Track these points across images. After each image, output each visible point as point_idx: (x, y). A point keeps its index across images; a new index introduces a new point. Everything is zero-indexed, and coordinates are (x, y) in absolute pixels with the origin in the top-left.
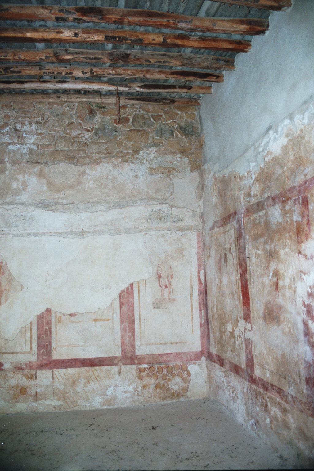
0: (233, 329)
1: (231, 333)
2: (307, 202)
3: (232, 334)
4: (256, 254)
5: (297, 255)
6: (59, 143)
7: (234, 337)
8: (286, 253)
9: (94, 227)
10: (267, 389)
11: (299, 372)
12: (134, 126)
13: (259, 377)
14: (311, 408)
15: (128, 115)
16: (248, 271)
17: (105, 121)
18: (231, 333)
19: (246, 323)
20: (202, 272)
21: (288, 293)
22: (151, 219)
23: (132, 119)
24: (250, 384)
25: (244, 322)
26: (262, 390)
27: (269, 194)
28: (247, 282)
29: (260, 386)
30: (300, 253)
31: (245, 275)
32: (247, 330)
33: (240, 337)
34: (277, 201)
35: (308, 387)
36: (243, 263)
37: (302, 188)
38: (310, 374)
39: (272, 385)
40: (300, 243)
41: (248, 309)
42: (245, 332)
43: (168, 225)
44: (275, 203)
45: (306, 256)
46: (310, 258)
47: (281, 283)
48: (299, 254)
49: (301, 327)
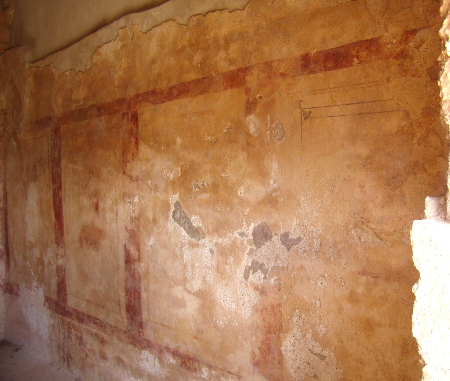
0: (41, 255)
1: (39, 259)
3: (41, 261)
4: (73, 169)
7: (43, 264)
8: (109, 171)
11: (119, 300)
13: (73, 309)
14: (131, 336)
16: (63, 189)
18: (39, 259)
19: (58, 247)
21: (109, 215)
24: (61, 316)
25: (56, 247)
26: (77, 323)
27: (94, 102)
28: (60, 200)
29: (74, 318)
30: (124, 173)
32: (59, 256)
33: (50, 263)
35: (128, 315)
38: (131, 302)
39: (89, 316)
40: (125, 162)
42: (57, 258)
46: (135, 180)
47: (101, 205)
48: (124, 175)
49: (122, 253)
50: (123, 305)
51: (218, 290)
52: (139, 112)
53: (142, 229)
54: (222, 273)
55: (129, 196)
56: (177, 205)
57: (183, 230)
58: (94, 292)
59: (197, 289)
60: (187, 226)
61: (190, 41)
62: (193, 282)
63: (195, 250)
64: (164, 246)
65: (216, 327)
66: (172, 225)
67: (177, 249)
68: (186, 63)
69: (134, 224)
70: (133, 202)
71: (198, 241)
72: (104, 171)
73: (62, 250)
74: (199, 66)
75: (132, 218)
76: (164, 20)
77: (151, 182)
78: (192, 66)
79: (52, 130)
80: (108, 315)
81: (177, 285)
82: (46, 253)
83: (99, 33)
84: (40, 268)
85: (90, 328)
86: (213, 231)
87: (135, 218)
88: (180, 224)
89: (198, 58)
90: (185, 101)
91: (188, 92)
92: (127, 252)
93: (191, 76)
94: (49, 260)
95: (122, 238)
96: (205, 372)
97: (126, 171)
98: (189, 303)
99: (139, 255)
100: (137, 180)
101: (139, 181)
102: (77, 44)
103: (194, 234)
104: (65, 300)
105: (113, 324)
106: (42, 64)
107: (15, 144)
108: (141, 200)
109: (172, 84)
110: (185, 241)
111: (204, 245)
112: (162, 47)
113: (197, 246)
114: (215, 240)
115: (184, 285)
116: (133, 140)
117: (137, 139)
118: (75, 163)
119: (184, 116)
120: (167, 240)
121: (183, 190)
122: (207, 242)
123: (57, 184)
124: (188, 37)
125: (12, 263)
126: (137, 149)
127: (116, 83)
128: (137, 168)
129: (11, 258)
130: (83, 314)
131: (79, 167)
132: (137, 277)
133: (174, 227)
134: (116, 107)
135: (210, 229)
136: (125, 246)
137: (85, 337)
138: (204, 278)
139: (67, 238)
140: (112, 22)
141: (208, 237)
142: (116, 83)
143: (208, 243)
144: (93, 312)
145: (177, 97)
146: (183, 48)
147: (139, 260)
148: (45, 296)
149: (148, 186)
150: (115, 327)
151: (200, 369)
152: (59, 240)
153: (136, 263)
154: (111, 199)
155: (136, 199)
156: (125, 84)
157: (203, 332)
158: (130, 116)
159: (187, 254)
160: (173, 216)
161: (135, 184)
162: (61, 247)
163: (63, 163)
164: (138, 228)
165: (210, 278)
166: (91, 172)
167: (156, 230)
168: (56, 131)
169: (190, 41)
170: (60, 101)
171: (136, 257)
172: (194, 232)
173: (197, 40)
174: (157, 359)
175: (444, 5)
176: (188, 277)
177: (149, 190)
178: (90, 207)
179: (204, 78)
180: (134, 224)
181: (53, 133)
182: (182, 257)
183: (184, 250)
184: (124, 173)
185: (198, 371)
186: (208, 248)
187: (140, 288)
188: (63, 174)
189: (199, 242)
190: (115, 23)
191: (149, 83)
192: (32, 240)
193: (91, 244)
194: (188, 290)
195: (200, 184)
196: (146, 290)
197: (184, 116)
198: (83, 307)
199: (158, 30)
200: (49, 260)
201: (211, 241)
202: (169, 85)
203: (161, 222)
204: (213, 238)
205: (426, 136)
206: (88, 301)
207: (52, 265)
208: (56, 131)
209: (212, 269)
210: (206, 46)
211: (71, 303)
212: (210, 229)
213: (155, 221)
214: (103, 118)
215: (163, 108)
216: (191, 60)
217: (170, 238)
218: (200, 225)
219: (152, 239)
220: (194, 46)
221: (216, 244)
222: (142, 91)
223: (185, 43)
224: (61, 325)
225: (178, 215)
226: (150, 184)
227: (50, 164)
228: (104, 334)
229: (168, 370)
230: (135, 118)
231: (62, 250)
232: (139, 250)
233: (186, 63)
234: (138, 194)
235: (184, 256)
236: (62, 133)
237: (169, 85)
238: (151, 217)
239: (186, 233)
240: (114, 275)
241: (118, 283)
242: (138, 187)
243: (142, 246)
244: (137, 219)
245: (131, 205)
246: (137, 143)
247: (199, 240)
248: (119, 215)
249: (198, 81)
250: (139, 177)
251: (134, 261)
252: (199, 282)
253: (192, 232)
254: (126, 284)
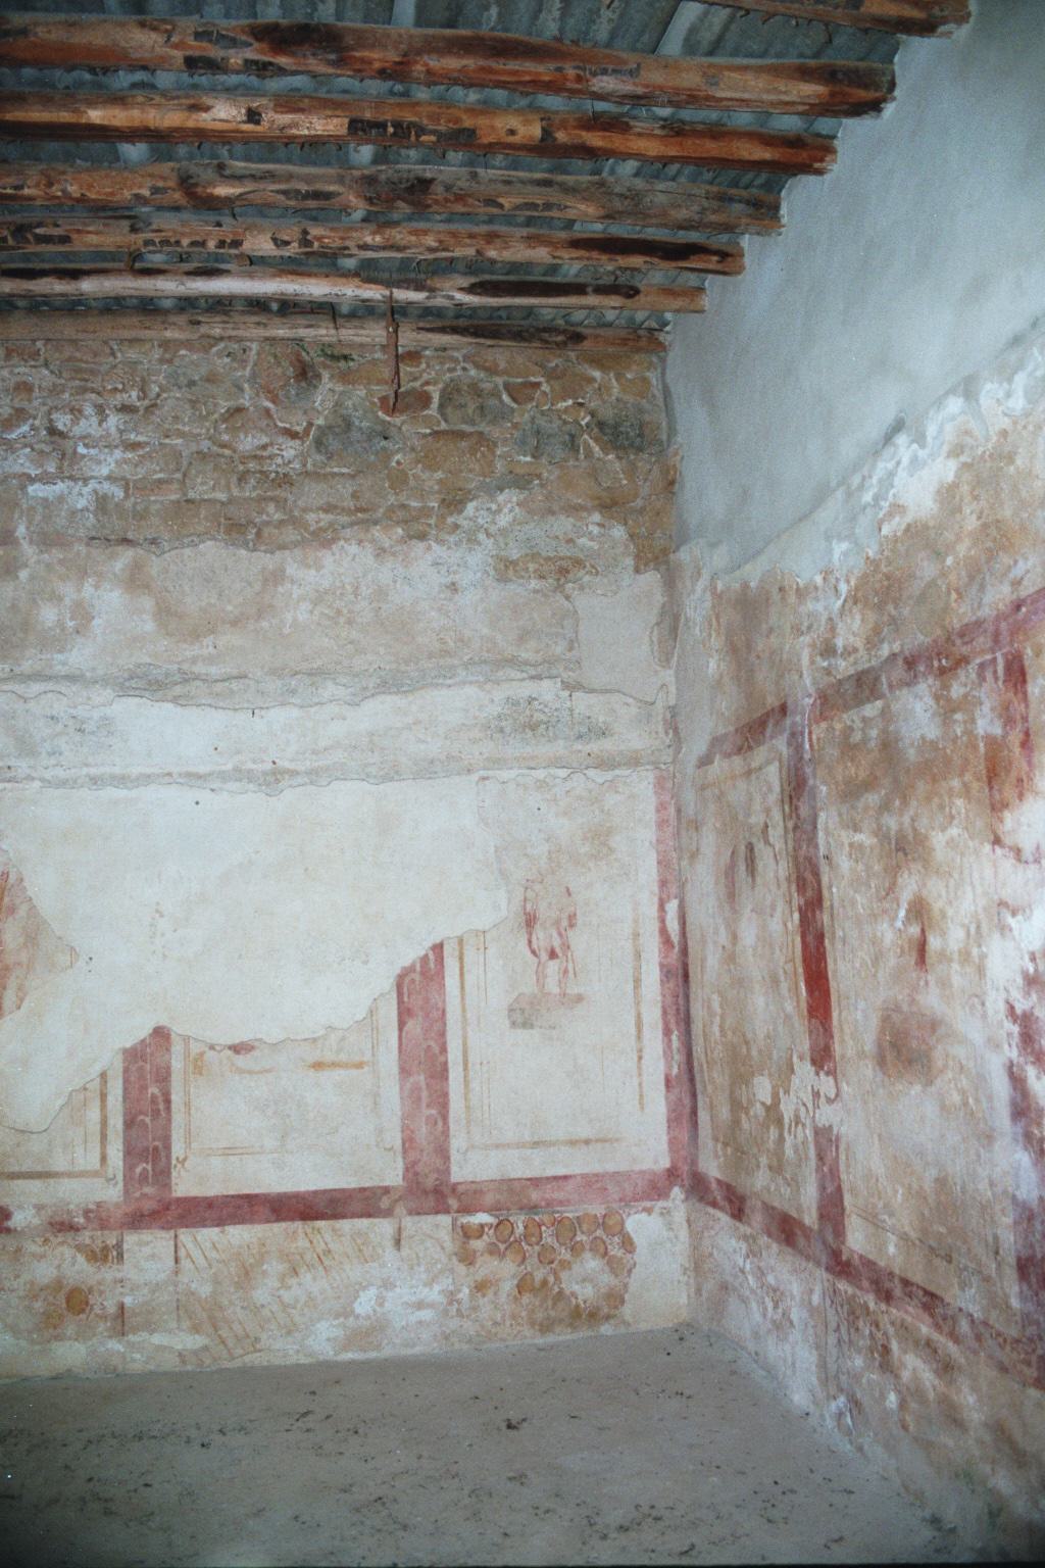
0: (775, 1096)
1: (768, 1109)
2: (1023, 673)
3: (773, 1111)
4: (851, 845)
5: (987, 847)
6: (197, 476)
7: (779, 1121)
8: (951, 843)
9: (314, 757)
10: (887, 1297)
11: (996, 1238)
12: (446, 421)
13: (861, 1257)
14: (1034, 1359)
15: (427, 383)
16: (826, 904)
17: (350, 403)
18: (768, 1109)
19: (817, 1074)
20: (672, 907)
21: (958, 977)
22: (502, 730)
23: (441, 397)
24: (831, 1277)
25: (812, 1073)
26: (870, 1300)
27: (896, 647)
28: (820, 937)
29: (866, 1284)
30: (997, 841)
31: (814, 916)
32: (823, 1099)
33: (797, 1121)
34: (922, 668)
35: (1025, 1288)
36: (809, 876)
37: (1003, 625)
38: (1032, 1246)
39: (906, 1283)
40: (997, 807)
41: (826, 1030)
42: (816, 1106)
43: (559, 748)
44: (915, 676)
45: (1018, 852)
46: (1031, 859)
47: (934, 943)
48: (996, 847)
49: (1001, 1088)
175: (336, 290)
205: (775, 1163)
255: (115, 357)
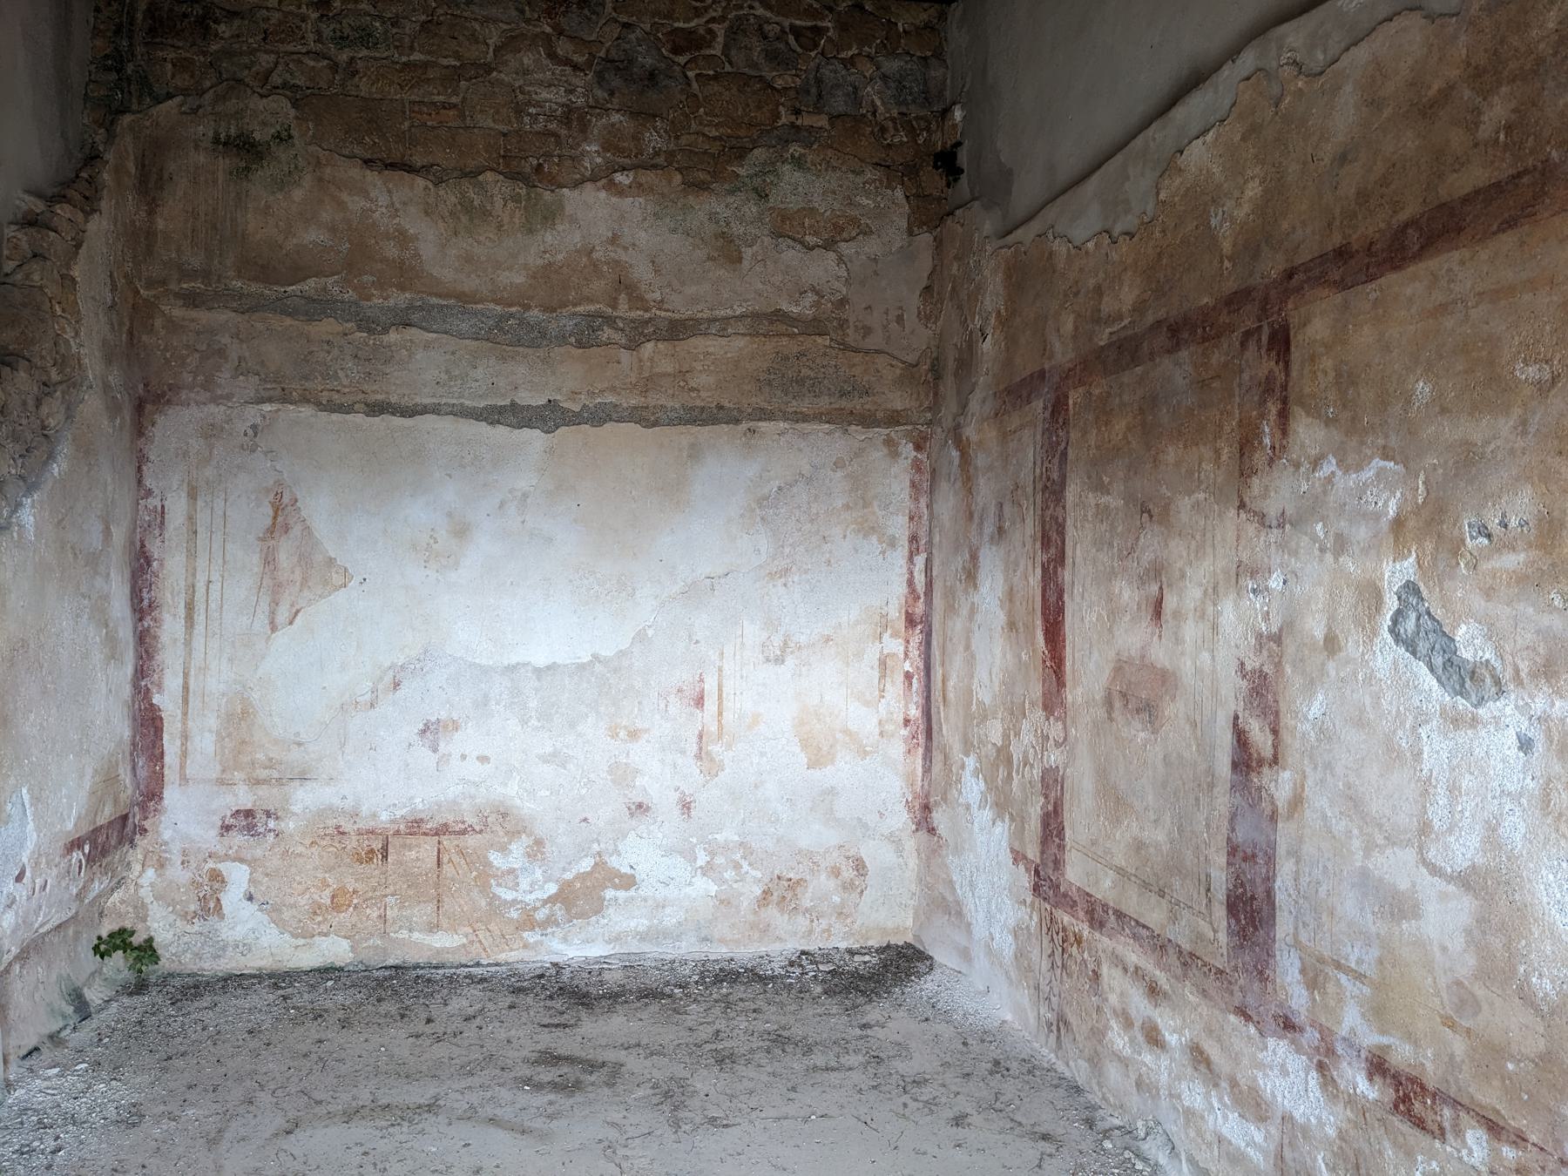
0: (1006, 737)
2: (1287, 342)
5: (1232, 512)
10: (1097, 923)
11: (1208, 876)
12: (730, 63)
15: (713, 20)
16: (1069, 561)
17: (632, 36)
18: (999, 751)
20: (920, 560)
22: (770, 383)
23: (726, 36)
27: (1162, 314)
29: (1081, 914)
30: (1242, 506)
31: (1055, 572)
32: (1051, 742)
34: (1186, 335)
35: (1233, 921)
36: (1054, 536)
37: (1273, 292)
38: (1242, 885)
39: (1120, 915)
40: (1245, 473)
41: (1058, 679)
43: (824, 403)
44: (1178, 344)
45: (1262, 518)
46: (1274, 523)
47: (1170, 602)
49: (1226, 739)
50: (1220, 894)
51: (1544, 872)
52: (1294, 321)
53: (1288, 670)
54: (1561, 815)
55: (1253, 573)
56: (1411, 588)
57: (1425, 670)
58: (1139, 846)
59: (1467, 864)
60: (1438, 661)
61: (1469, 64)
62: (1452, 839)
63: (1464, 736)
64: (1360, 722)
65: (1526, 997)
66: (1386, 655)
67: (1400, 733)
68: (1457, 139)
69: (1265, 653)
70: (1267, 589)
71: (1476, 707)
72: (1184, 504)
73: (1060, 725)
74: (1502, 137)
75: (1259, 636)
76: (1380, 18)
77: (1324, 526)
78: (1476, 145)
79: (1045, 408)
80: (1174, 919)
81: (1394, 844)
82: (1017, 734)
83: (1179, 113)
84: (1002, 773)
85: (1120, 949)
86: (1534, 675)
87: (1271, 638)
88: (1414, 653)
89: (1497, 111)
90: (1446, 262)
91: (1460, 230)
92: (1241, 739)
93: (1477, 176)
94: (1025, 754)
95: (1230, 693)
96: (1476, 1145)
97: (1247, 500)
98: (1431, 909)
99: (1275, 747)
100: (1281, 526)
101: (1288, 526)
102: (1119, 157)
103: (1463, 685)
104: (1058, 864)
105: (1186, 947)
106: (1025, 234)
107: (955, 454)
108: (1304, 584)
109: (1404, 216)
110: (1433, 708)
111: (1496, 720)
112: (1374, 104)
113: (1474, 722)
114: (1539, 705)
115: (1421, 848)
116: (1273, 408)
117: (1285, 401)
118: (1101, 488)
119: (1442, 309)
120: (1368, 701)
121: (1429, 546)
122: (1508, 710)
123: (1053, 550)
124: (1464, 51)
125: (937, 757)
126: (1285, 433)
127: (1227, 247)
128: (1280, 490)
129: (935, 744)
130: (1105, 907)
131: (1114, 501)
132: (1268, 812)
133: (1395, 663)
134: (1224, 318)
135: (1524, 667)
136: (1236, 718)
137: (1105, 970)
138: (1492, 830)
139: (1074, 694)
140: (1218, 67)
141: (1513, 697)
142: (1227, 247)
143: (1507, 717)
144: (1133, 903)
145: (1418, 256)
146: (1447, 93)
147: (1275, 760)
148: (1012, 850)
149: (1314, 539)
150: (1191, 954)
151: (1459, 1133)
152: (1053, 702)
153: (1265, 770)
154: (1201, 585)
155: (1275, 582)
156: (1252, 246)
157: (1477, 1008)
158: (1265, 339)
159: (1436, 749)
160: (1392, 631)
161: (1275, 534)
162: (1057, 719)
163: (1072, 493)
164: (1278, 666)
165: (1515, 828)
166: (1145, 510)
167: (1333, 673)
168: (1058, 407)
169: (1469, 64)
170: (1068, 325)
171: (1268, 752)
172: (1462, 677)
173: (1496, 52)
174: (1314, 1074)
176: (1436, 824)
177: (1317, 553)
178: (1139, 608)
179: (1519, 175)
180: (1265, 653)
181: (1047, 414)
182: (1418, 756)
183: (1424, 736)
184: (1242, 506)
185: (1449, 1136)
186: (1512, 732)
187: (1272, 845)
188: (1069, 522)
189: (1481, 711)
190: (1226, 71)
191: (1330, 225)
192: (986, 698)
193: (1138, 711)
194: (1434, 865)
195: (1494, 525)
196: (1295, 854)
197: (1442, 309)
198: (1105, 888)
199: (1361, 54)
200: (1025, 754)
201: (1523, 709)
202: (1394, 221)
203: (1352, 645)
204: (1532, 697)
206: (1120, 871)
207: (1032, 766)
208: (1058, 407)
209: (1524, 801)
210: (1527, 67)
211: (1075, 873)
212: (1524, 667)
213: (1331, 644)
214: (1184, 354)
215: (1373, 296)
216: (1473, 125)
217: (1377, 698)
218: (1487, 656)
219: (1320, 697)
220: (1483, 77)
221: (1543, 719)
222: (1305, 256)
223: (1454, 73)
224: (1045, 929)
225: (1410, 625)
226: (1321, 535)
227: (1039, 497)
228: (1158, 973)
229: (1348, 1112)
230: (1281, 343)
231: (1060, 725)
232: (1275, 732)
233: (1457, 139)
234: (1281, 566)
235: (1425, 756)
236: (1071, 412)
237: (1394, 221)
238: (1319, 633)
239: (1434, 682)
240: (1197, 799)
241: (1208, 826)
242: (1282, 546)
243: (1287, 720)
244: (1277, 639)
245: (1260, 598)
246: (1284, 415)
247: (1481, 701)
248: (1221, 630)
249: (1496, 189)
250: (1288, 513)
251: (1261, 762)
252: (1474, 841)
253: (1455, 677)
254: (1233, 830)
255: (614, 308)
